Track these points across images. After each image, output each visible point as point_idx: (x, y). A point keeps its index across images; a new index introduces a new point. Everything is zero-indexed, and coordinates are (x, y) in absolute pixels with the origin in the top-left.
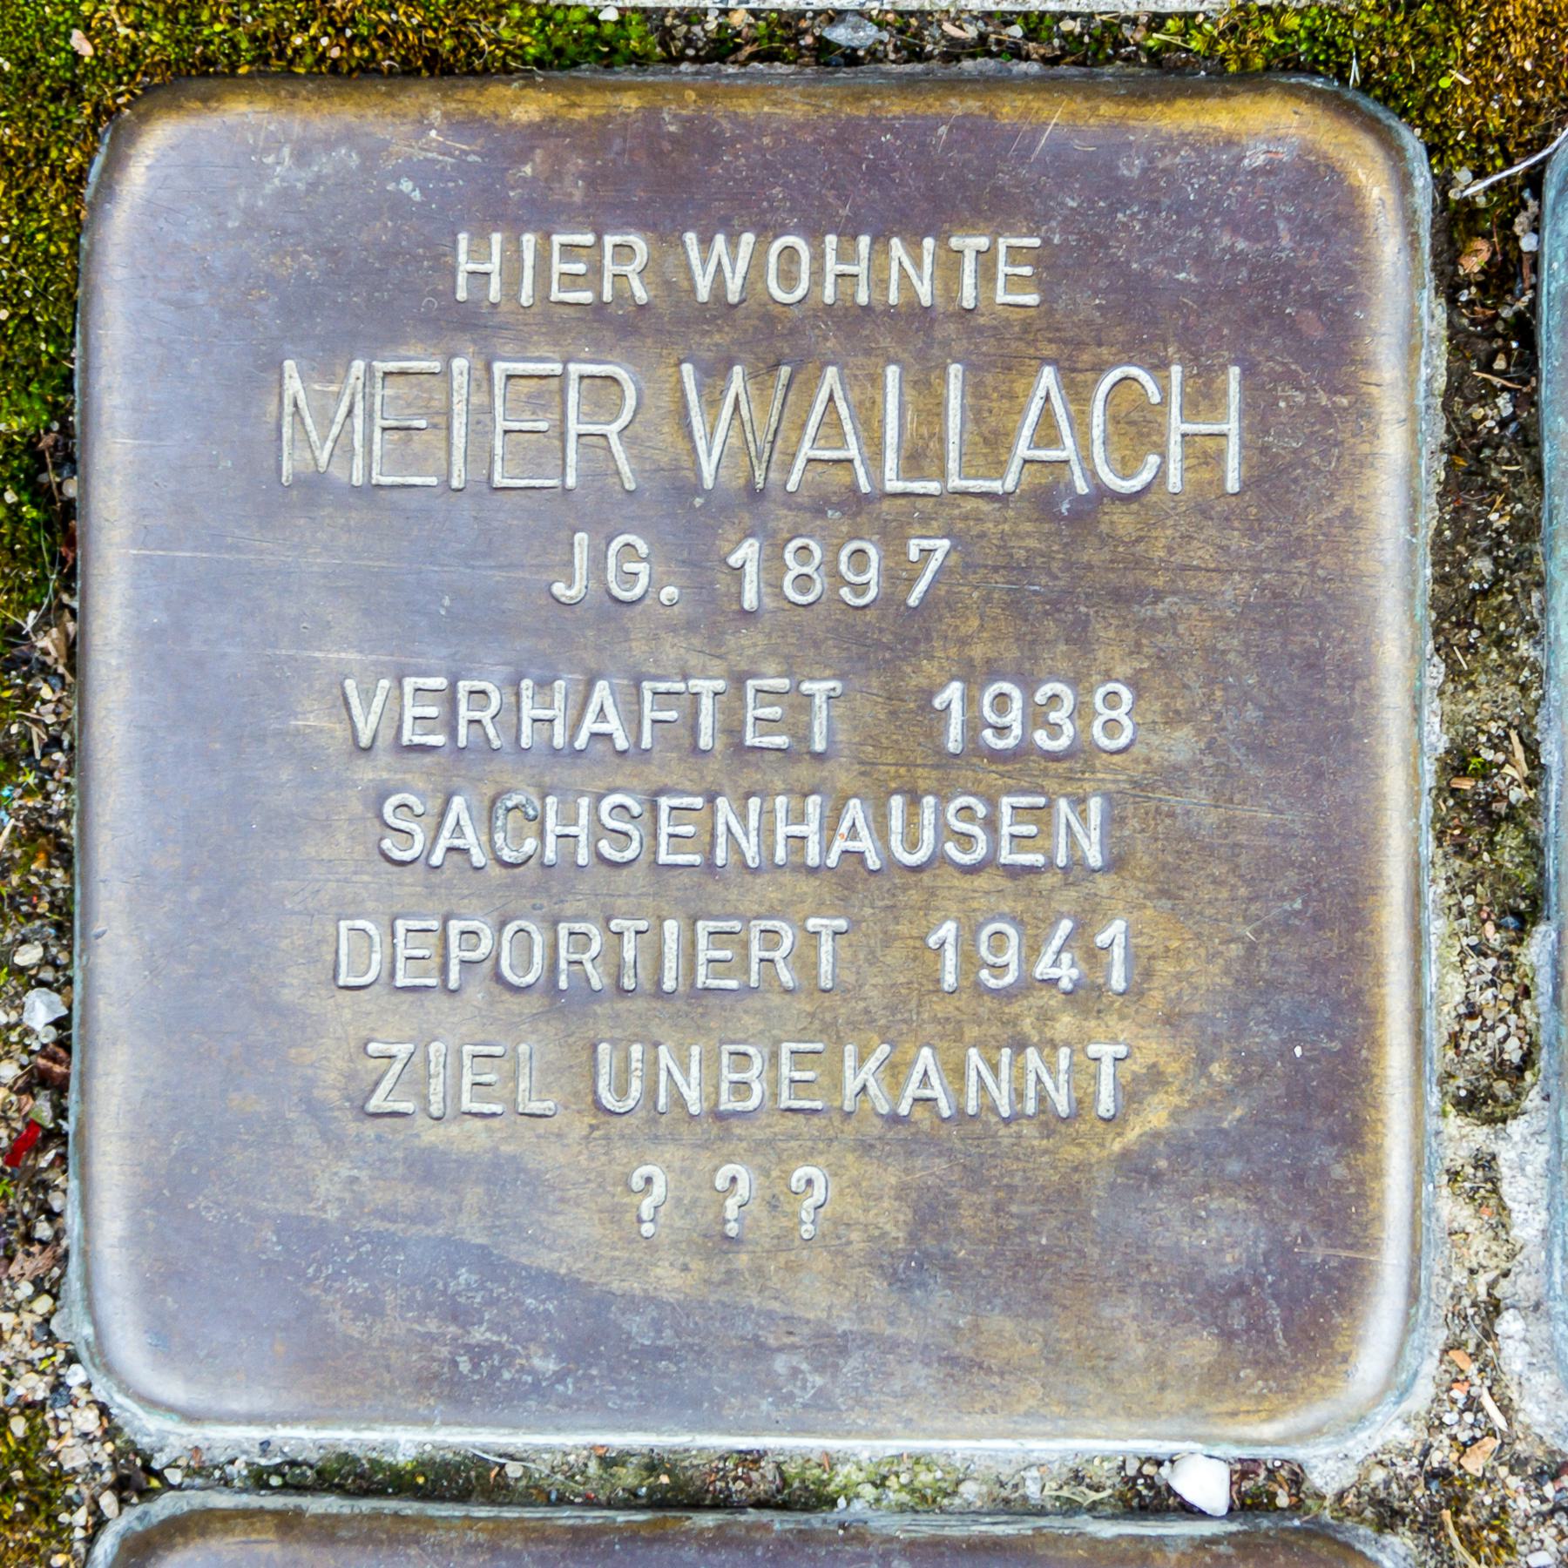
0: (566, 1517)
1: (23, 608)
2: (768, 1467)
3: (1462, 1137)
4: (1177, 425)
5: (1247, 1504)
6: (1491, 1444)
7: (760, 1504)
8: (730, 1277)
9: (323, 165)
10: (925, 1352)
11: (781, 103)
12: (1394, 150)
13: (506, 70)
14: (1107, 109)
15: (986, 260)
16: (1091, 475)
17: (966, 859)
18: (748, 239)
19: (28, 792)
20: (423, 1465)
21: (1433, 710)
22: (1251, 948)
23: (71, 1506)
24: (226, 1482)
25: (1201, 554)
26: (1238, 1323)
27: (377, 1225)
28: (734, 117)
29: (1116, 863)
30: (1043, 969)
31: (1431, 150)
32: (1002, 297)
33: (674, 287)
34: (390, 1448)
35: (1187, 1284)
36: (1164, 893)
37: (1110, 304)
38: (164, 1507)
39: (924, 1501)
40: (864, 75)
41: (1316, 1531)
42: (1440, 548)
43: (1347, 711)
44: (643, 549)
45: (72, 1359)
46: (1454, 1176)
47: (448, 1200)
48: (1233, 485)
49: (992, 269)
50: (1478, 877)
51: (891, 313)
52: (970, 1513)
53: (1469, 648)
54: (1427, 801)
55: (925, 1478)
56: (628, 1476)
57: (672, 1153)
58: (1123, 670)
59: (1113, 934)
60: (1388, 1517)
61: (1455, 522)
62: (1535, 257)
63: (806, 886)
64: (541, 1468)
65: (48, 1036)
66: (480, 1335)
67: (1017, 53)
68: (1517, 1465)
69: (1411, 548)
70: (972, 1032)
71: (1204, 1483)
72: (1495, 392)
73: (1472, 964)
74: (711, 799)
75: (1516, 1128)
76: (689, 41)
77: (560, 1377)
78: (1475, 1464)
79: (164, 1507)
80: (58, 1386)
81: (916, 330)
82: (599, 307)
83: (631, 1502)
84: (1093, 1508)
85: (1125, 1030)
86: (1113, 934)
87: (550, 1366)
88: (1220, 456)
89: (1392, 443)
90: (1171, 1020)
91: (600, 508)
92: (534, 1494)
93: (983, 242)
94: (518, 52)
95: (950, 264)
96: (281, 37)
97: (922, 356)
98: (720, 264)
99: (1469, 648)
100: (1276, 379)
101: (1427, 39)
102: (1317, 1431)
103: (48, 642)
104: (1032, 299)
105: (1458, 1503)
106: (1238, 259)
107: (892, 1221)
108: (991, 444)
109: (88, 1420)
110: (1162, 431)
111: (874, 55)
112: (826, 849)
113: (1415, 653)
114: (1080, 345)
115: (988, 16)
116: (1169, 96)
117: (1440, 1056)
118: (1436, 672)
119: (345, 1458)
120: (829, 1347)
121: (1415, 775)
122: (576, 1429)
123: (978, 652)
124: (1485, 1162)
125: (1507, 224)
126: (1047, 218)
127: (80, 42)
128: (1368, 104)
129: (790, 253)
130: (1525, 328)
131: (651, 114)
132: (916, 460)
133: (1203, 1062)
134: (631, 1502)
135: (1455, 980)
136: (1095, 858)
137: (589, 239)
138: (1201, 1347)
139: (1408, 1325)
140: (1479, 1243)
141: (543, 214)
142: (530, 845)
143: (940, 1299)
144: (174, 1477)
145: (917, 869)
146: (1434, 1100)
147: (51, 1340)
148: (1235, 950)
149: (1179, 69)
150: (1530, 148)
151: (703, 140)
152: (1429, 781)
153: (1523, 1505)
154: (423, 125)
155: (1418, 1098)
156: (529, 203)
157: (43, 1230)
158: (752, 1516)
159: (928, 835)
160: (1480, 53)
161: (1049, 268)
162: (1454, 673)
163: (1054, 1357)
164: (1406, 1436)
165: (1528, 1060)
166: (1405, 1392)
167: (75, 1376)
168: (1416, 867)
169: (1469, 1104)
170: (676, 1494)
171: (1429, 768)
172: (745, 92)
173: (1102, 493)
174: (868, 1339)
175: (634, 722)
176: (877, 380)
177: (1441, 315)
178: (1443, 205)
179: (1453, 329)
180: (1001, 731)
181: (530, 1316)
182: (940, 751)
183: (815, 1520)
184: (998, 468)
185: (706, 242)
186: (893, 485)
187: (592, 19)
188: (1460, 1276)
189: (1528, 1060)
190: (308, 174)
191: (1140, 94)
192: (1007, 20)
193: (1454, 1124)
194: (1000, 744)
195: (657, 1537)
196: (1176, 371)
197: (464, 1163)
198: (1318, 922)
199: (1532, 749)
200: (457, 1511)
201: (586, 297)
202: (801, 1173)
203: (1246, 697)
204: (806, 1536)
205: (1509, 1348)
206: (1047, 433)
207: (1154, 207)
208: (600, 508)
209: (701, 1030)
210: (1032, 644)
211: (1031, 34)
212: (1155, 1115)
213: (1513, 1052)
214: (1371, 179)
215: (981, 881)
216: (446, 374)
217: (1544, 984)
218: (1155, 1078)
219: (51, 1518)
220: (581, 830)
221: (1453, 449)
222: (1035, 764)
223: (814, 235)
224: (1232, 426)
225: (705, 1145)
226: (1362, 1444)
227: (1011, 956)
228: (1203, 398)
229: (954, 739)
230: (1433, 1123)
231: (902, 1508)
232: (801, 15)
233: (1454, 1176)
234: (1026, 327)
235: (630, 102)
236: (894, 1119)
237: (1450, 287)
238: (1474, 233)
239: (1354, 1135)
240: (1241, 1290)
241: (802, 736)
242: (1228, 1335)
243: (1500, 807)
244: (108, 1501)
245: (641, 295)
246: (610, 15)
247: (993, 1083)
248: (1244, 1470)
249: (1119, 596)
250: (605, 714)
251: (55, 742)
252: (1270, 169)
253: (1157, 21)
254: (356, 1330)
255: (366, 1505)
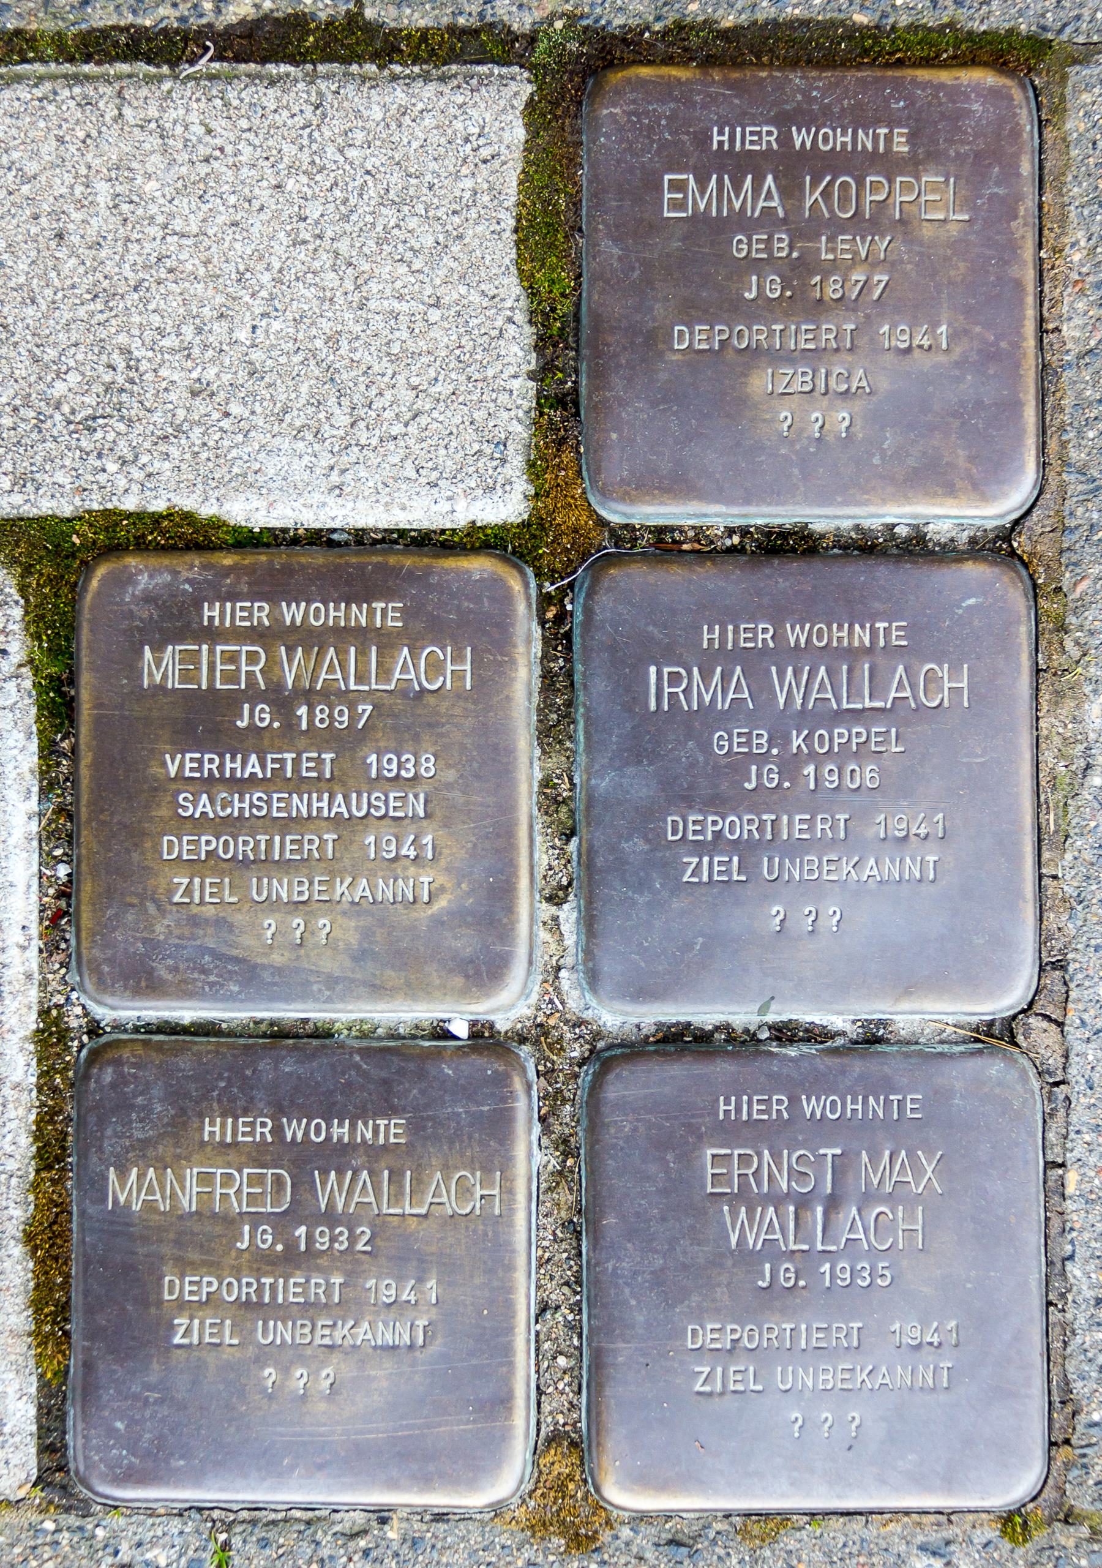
0: (242, 1041)
1: (56, 734)
2: (311, 1024)
3: (546, 910)
4: (450, 667)
5: (475, 1035)
6: (558, 1015)
7: (309, 1036)
8: (298, 958)
9: (159, 580)
10: (364, 983)
11: (317, 558)
12: (523, 574)
13: (221, 548)
14: (425, 560)
15: (384, 611)
16: (420, 684)
17: (378, 814)
18: (303, 604)
19: (58, 796)
20: (193, 1024)
21: (537, 765)
22: (475, 845)
23: (72, 1040)
24: (126, 1031)
25: (458, 711)
26: (471, 972)
27: (177, 941)
28: (299, 563)
29: (428, 816)
30: (404, 852)
31: (536, 575)
32: (390, 624)
33: (276, 617)
34: (181, 1018)
35: (453, 959)
36: (445, 826)
37: (425, 626)
38: (103, 1040)
39: (364, 1035)
40: (344, 550)
41: (498, 1044)
42: (540, 711)
43: (508, 763)
44: (267, 709)
45: (73, 990)
46: (545, 923)
47: (201, 932)
48: (468, 687)
49: (387, 614)
50: (552, 823)
51: (353, 629)
52: (380, 1038)
53: (549, 744)
54: (535, 796)
55: (365, 1027)
56: (263, 1027)
57: (277, 915)
58: (432, 750)
59: (427, 839)
60: (523, 1040)
61: (544, 702)
62: (572, 612)
63: (324, 824)
64: (233, 1025)
65: (65, 879)
66: (212, 978)
67: (396, 542)
68: (566, 1022)
69: (529, 709)
70: (380, 874)
71: (460, 1029)
72: (558, 658)
73: (551, 852)
74: (290, 795)
75: (566, 906)
76: (284, 539)
77: (239, 993)
78: (552, 1022)
79: (103, 1040)
80: (68, 999)
81: (362, 636)
82: (252, 627)
83: (264, 1036)
84: (422, 1037)
85: (432, 873)
86: (427, 839)
87: (236, 989)
88: (464, 677)
89: (522, 673)
90: (448, 870)
91: (253, 695)
92: (231, 1034)
93: (383, 605)
94: (225, 542)
95: (371, 613)
96: (144, 536)
97: (363, 644)
98: (293, 613)
99: (549, 744)
100: (483, 651)
101: (535, 537)
102: (498, 1009)
103: (65, 744)
104: (400, 624)
105: (546, 1034)
106: (471, 611)
107: (353, 939)
108: (384, 672)
109: (78, 1010)
110: (445, 670)
111: (347, 544)
112: (330, 811)
113: (531, 745)
114: (417, 640)
115: (385, 530)
116: (446, 556)
117: (540, 883)
118: (538, 752)
119: (166, 1022)
120: (331, 981)
121: (531, 786)
122: (245, 1011)
123: (382, 744)
124: (556, 919)
125: (562, 601)
126: (405, 597)
127: (75, 539)
128: (514, 559)
129: (317, 609)
130: (568, 636)
131: (271, 562)
132: (359, 679)
133: (459, 885)
134: (264, 1036)
135: (545, 857)
136: (422, 814)
137: (248, 604)
138: (459, 981)
139: (529, 973)
140: (553, 946)
141: (234, 597)
142: (229, 811)
143: (369, 964)
144: (108, 1029)
145: (361, 818)
146: (538, 897)
147: (66, 983)
148: (470, 845)
149: (452, 548)
150: (569, 575)
151: (288, 571)
152: (536, 789)
153: (569, 1035)
154: (192, 567)
155: (532, 896)
156: (228, 592)
157: (63, 946)
158: (305, 1040)
159: (365, 807)
160: (553, 542)
161: (406, 614)
162: (544, 752)
163: (408, 984)
164: (529, 1012)
165: (570, 884)
166: (528, 996)
167: (74, 996)
168: (531, 817)
169: (550, 899)
170: (279, 1034)
171: (536, 785)
172: (303, 555)
173: (423, 690)
174: (346, 978)
175: (263, 767)
176: (347, 652)
177: (540, 631)
178: (540, 594)
179: (544, 637)
180: (389, 771)
181: (230, 972)
182: (369, 778)
183: (327, 1041)
184: (388, 681)
185: (289, 606)
186: (353, 687)
187: (251, 531)
188: (547, 958)
189: (570, 884)
190: (153, 582)
191: (437, 556)
192: (392, 531)
193: (544, 905)
194: (390, 775)
195: (272, 1047)
196: (449, 649)
197: (206, 920)
198: (498, 836)
199: (571, 779)
200: (205, 1039)
201: (248, 624)
202: (321, 922)
203: (473, 759)
204: (324, 1046)
205: (563, 982)
206: (404, 669)
207: (442, 593)
208: (253, 695)
209: (287, 873)
210: (400, 742)
211: (400, 537)
212: (442, 903)
213: (565, 882)
214: (515, 584)
215: (383, 822)
216: (200, 651)
217: (575, 857)
218: (442, 889)
219: (65, 1044)
220: (246, 805)
221: (543, 677)
222: (402, 782)
223: (325, 603)
224: (468, 667)
225: (289, 913)
226: (514, 1014)
227: (393, 847)
228: (458, 658)
229: (374, 774)
230: (538, 905)
231: (357, 1037)
232: (321, 530)
233: (545, 923)
234: (398, 634)
235: (263, 558)
236: (353, 903)
237: (542, 623)
238: (550, 604)
239: (510, 909)
240: (472, 961)
241: (321, 773)
242: (467, 977)
243: (560, 799)
244: (85, 1038)
245: (267, 623)
246: (257, 530)
247: (385, 891)
248: (473, 1024)
249: (430, 725)
250: (253, 766)
251: (67, 779)
252: (482, 580)
253: (443, 532)
254: (170, 977)
255: (173, 1038)
